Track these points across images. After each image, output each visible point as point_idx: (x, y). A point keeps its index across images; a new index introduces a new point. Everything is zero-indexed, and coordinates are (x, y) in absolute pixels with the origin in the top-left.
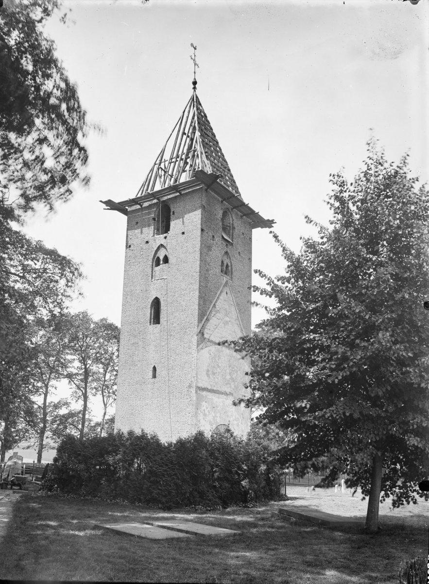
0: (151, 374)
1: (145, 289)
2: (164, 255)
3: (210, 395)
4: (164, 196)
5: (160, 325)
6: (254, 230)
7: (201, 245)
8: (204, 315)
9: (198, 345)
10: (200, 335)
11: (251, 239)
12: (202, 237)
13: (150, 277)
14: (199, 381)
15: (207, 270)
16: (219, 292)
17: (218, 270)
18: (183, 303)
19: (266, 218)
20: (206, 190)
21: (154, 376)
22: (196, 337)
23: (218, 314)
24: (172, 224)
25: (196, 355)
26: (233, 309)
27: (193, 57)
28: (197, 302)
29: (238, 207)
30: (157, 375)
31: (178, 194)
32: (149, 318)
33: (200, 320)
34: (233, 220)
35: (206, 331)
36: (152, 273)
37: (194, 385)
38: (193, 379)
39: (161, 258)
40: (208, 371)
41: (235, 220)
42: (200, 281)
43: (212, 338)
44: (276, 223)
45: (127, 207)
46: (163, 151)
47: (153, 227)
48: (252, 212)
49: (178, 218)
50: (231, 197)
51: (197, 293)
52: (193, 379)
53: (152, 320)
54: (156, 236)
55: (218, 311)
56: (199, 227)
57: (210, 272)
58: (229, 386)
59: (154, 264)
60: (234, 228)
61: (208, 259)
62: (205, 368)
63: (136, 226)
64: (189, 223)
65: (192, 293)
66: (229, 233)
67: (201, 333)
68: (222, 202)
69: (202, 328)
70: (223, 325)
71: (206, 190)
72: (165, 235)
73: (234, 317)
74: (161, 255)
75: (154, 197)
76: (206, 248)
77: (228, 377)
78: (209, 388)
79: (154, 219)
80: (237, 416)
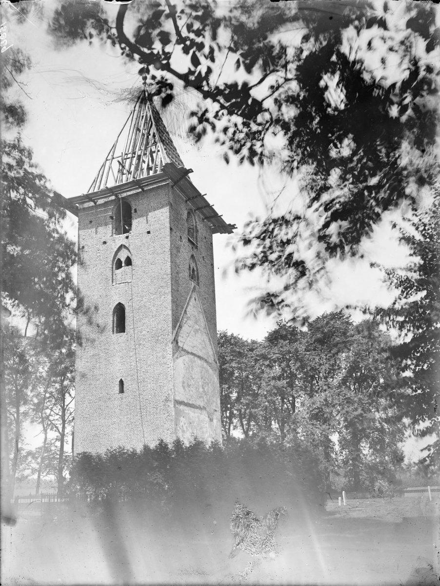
0: (117, 388)
1: (105, 295)
2: (126, 256)
3: (187, 410)
4: (124, 192)
5: (125, 333)
6: (213, 235)
7: (171, 245)
8: (177, 323)
9: (174, 354)
10: (175, 343)
11: (212, 244)
12: (171, 237)
13: (111, 281)
14: (176, 393)
15: (177, 273)
16: (188, 298)
17: (187, 274)
18: (153, 308)
19: (228, 223)
20: (172, 187)
21: (122, 391)
22: (171, 346)
23: (189, 321)
24: (135, 222)
25: (172, 365)
26: (201, 316)
27: (20, 84)
28: (170, 306)
29: (202, 208)
30: (125, 389)
31: (140, 190)
32: (111, 326)
33: (174, 327)
34: (196, 222)
35: (180, 339)
36: (113, 277)
37: (172, 398)
38: (170, 392)
39: (123, 260)
40: (184, 383)
41: (198, 222)
42: (172, 284)
43: (185, 347)
44: (237, 228)
45: (77, 205)
46: (114, 146)
47: (110, 226)
48: (216, 214)
49: (142, 216)
50: (196, 197)
51: (169, 298)
52: (170, 392)
53: (115, 329)
54: (114, 236)
55: (188, 318)
56: (168, 225)
57: (180, 275)
58: (202, 399)
59: (114, 267)
60: (197, 231)
61: (178, 261)
62: (181, 380)
63: (90, 226)
64: (155, 223)
65: (163, 297)
66: (193, 235)
67: (176, 341)
68: (186, 201)
69: (176, 336)
70: (194, 333)
71: (172, 187)
72: (126, 235)
73: (203, 325)
74: (123, 256)
75: (113, 192)
76: (175, 251)
77: (201, 390)
78: (186, 401)
79: (112, 218)
80: (211, 433)
